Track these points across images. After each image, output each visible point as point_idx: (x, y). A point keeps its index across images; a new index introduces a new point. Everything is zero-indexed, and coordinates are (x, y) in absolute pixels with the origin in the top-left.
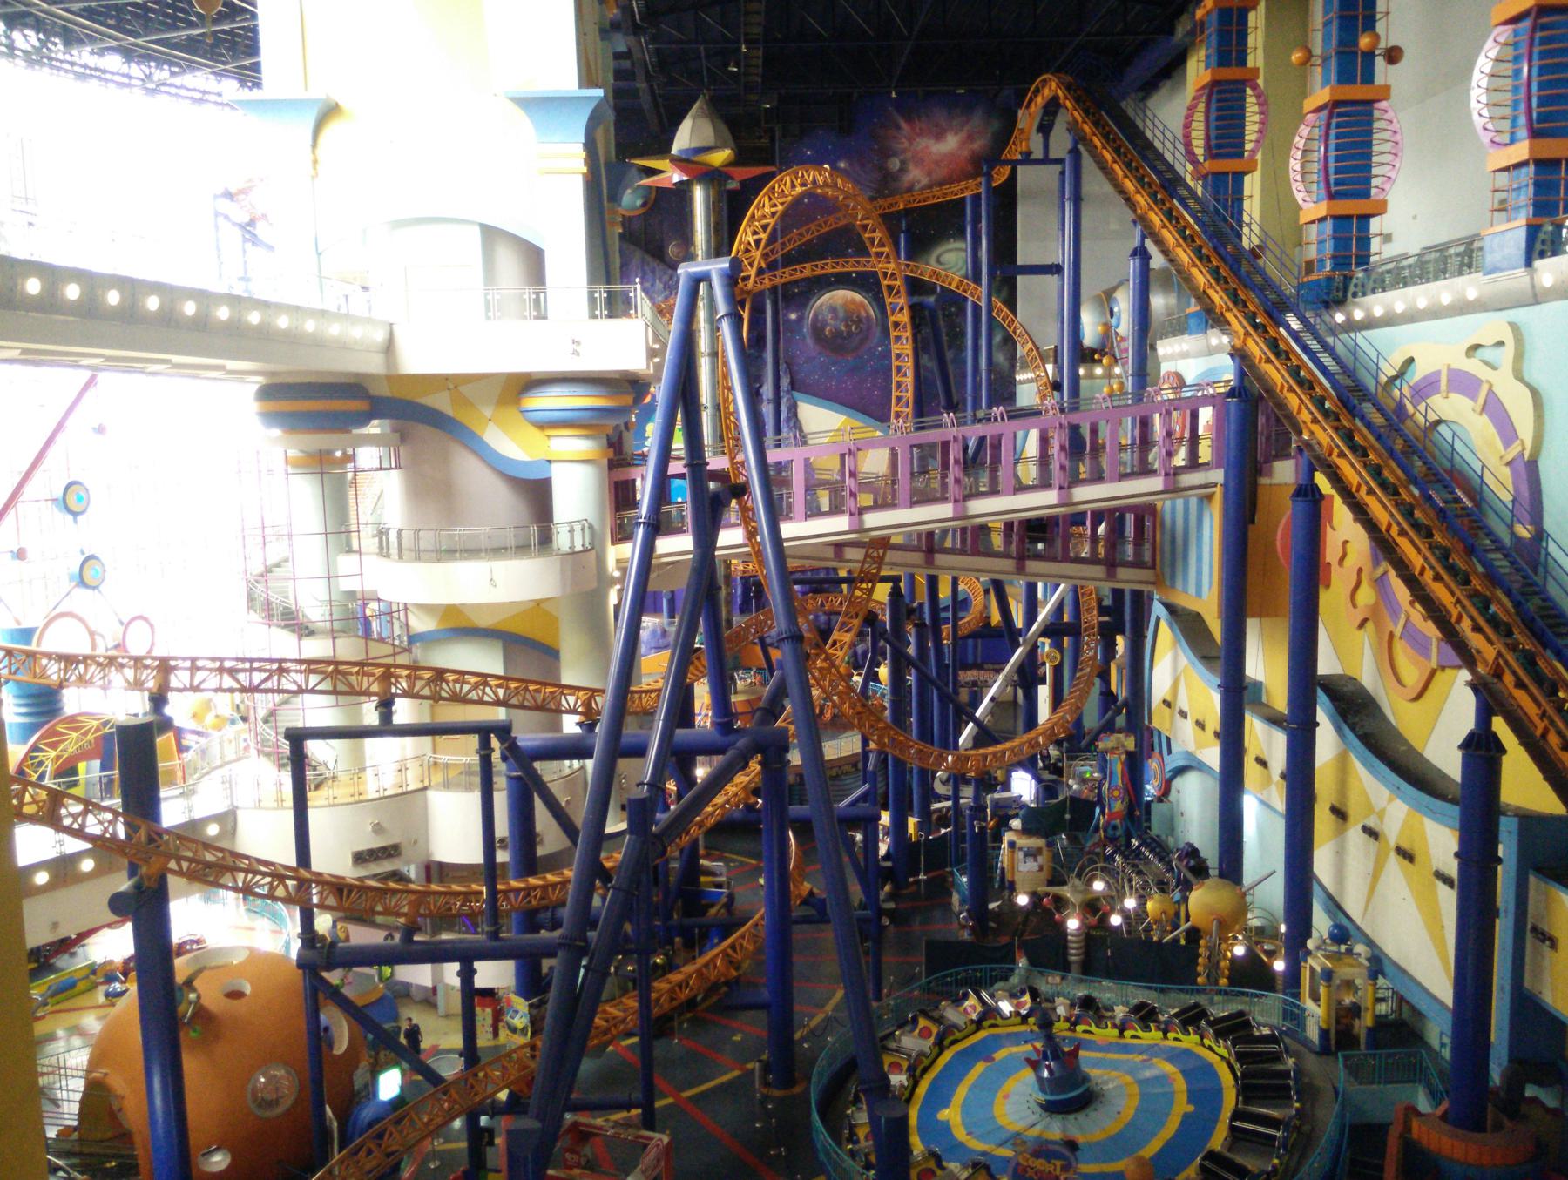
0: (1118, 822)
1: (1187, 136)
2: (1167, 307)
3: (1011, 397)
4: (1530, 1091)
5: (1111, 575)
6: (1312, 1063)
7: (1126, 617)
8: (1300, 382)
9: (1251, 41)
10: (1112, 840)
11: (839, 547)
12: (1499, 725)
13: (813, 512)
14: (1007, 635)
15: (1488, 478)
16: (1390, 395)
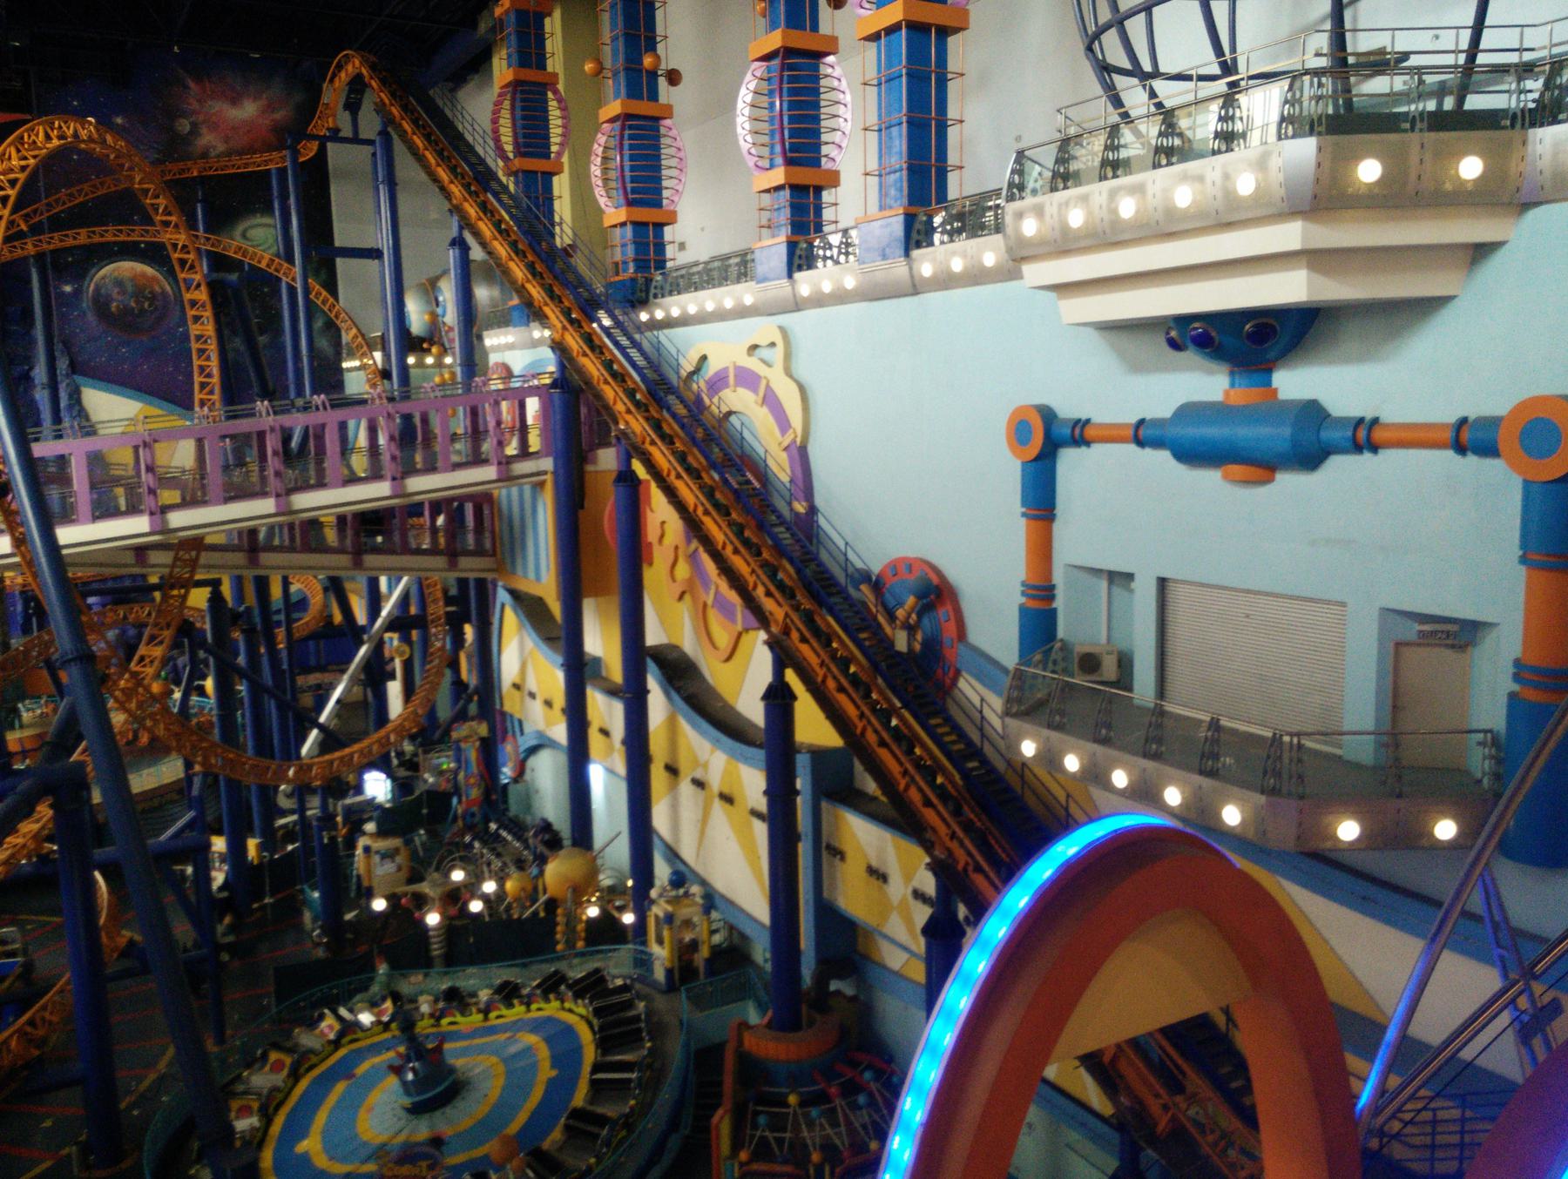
0: (475, 809)
1: (496, 131)
2: (492, 299)
3: (339, 385)
4: (834, 986)
5: (453, 565)
6: (661, 1002)
7: (471, 604)
8: (614, 375)
9: (549, 47)
10: (469, 828)
11: (140, 551)
12: (791, 676)
13: (104, 510)
14: (355, 634)
15: (771, 462)
16: (690, 389)
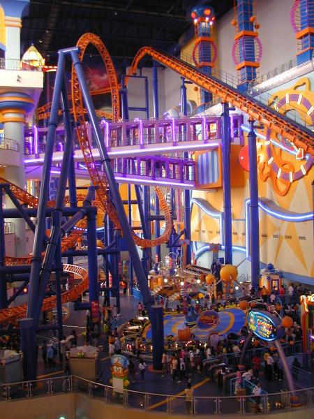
1: (194, 55)
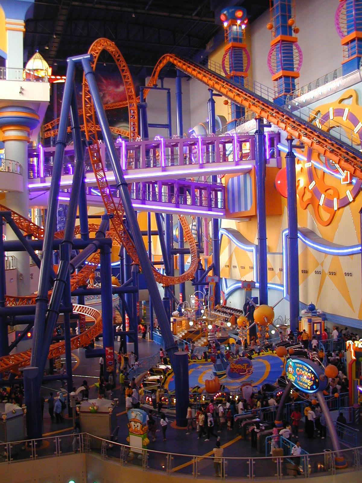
1: (223, 64)
